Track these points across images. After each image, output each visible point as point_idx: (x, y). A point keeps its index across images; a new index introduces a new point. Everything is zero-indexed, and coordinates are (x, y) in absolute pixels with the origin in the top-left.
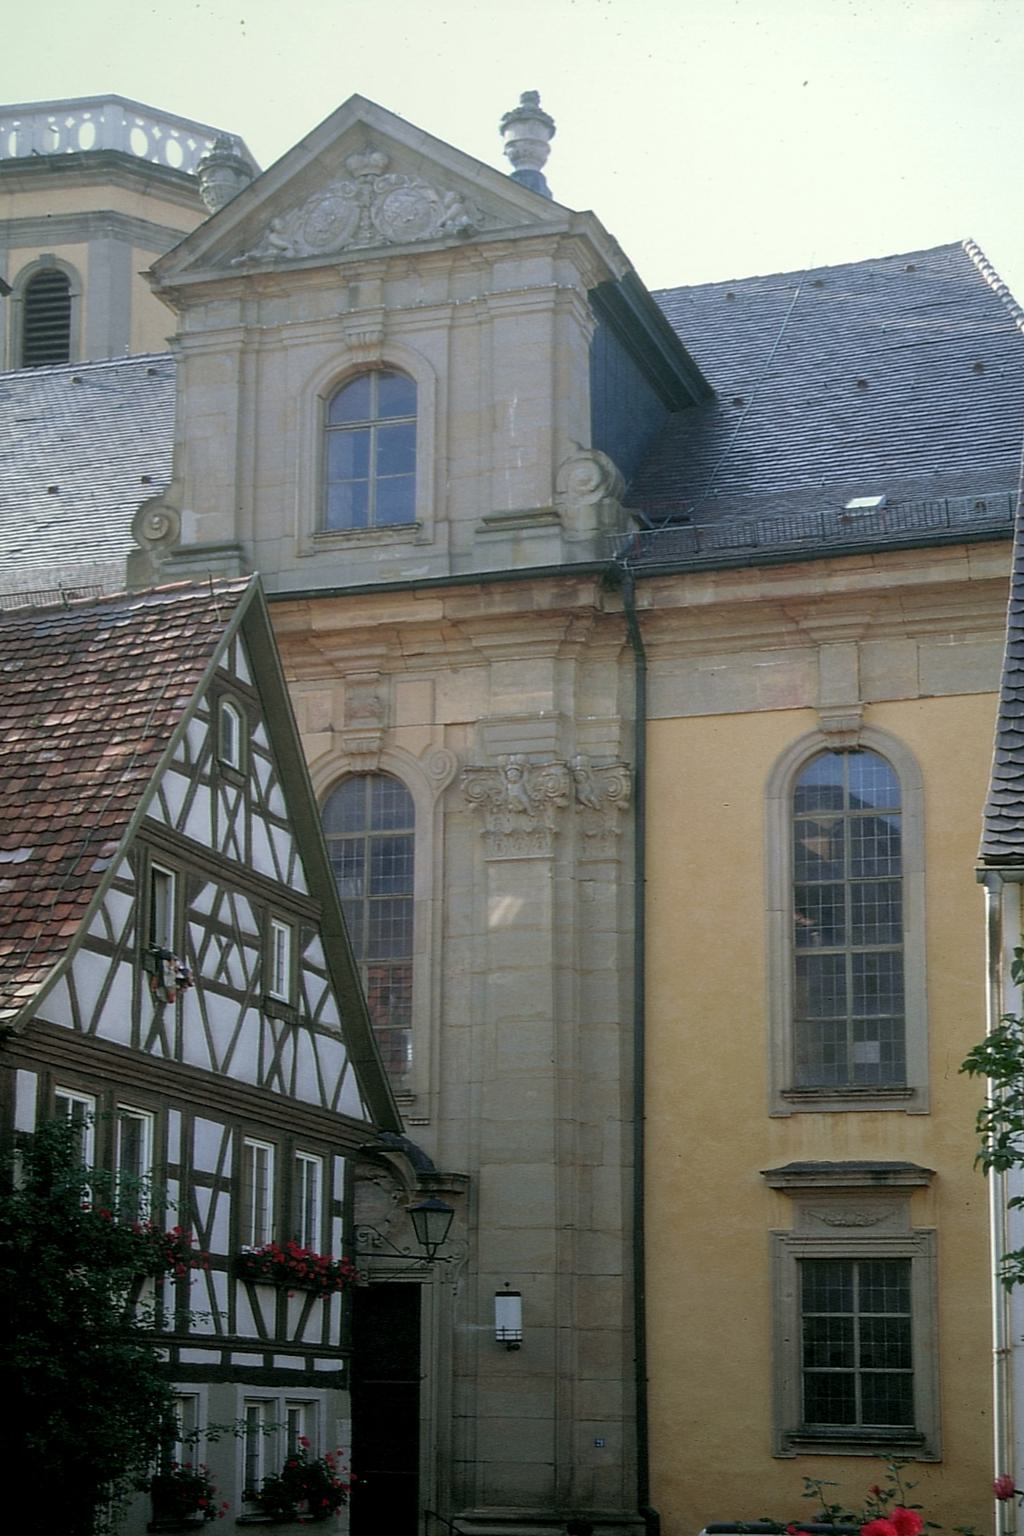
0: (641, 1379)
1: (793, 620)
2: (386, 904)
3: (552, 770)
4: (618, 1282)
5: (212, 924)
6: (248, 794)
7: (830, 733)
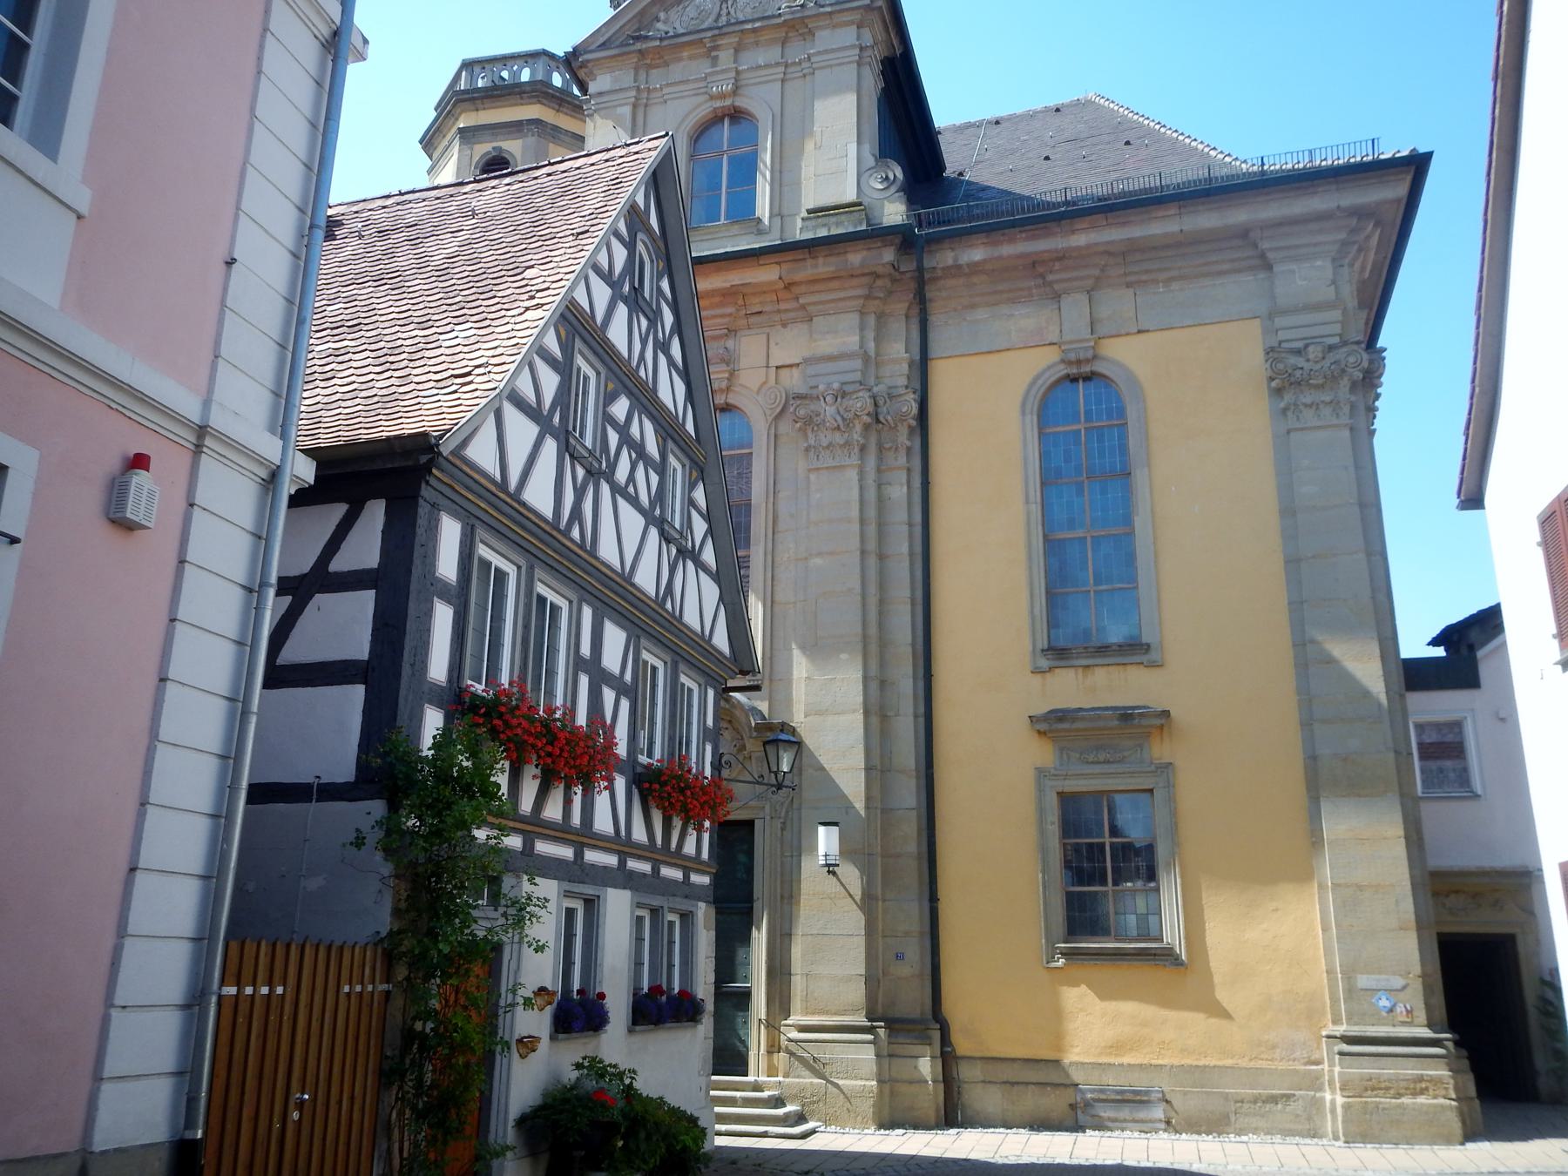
3: (861, 394)
4: (914, 813)
7: (1070, 363)
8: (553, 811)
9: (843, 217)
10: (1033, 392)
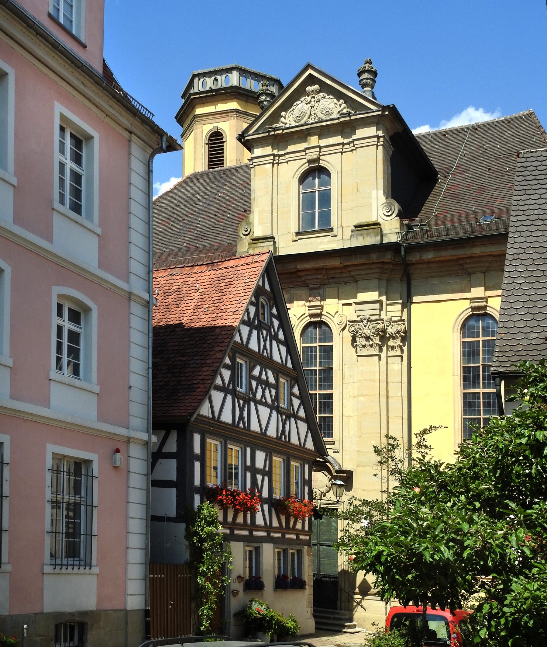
2: (324, 370)
5: (259, 380)
6: (271, 333)
8: (240, 520)
9: (370, 231)
10: (461, 317)
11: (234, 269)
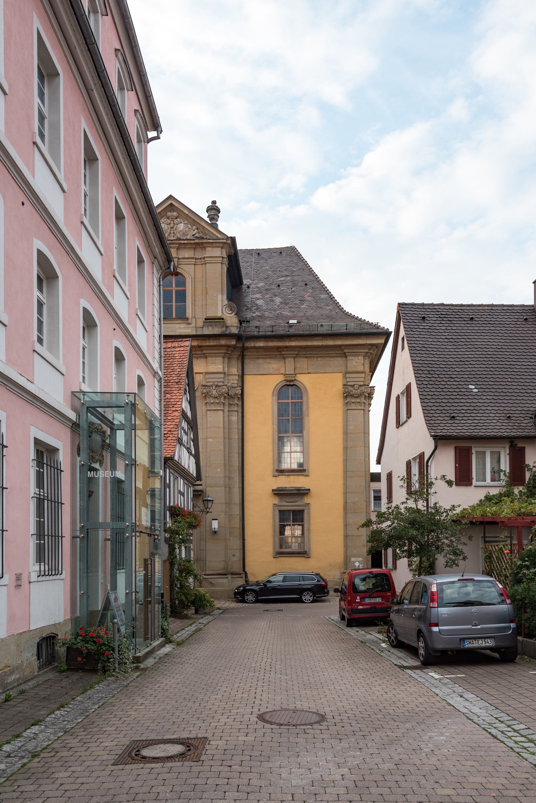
0: (244, 540)
1: (280, 352)
7: (287, 381)
11: (172, 349)
